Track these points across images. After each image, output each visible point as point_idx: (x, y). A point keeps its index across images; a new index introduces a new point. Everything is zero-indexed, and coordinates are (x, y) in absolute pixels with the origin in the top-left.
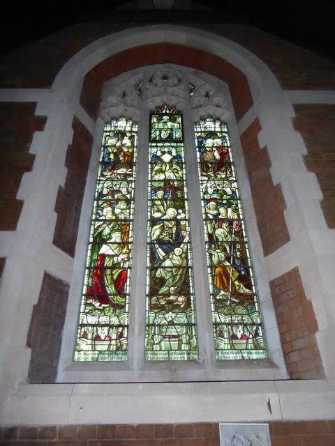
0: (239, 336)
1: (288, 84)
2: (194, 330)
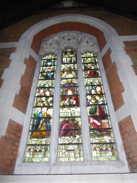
0: (104, 149)
1: (121, 33)
2: (81, 147)
